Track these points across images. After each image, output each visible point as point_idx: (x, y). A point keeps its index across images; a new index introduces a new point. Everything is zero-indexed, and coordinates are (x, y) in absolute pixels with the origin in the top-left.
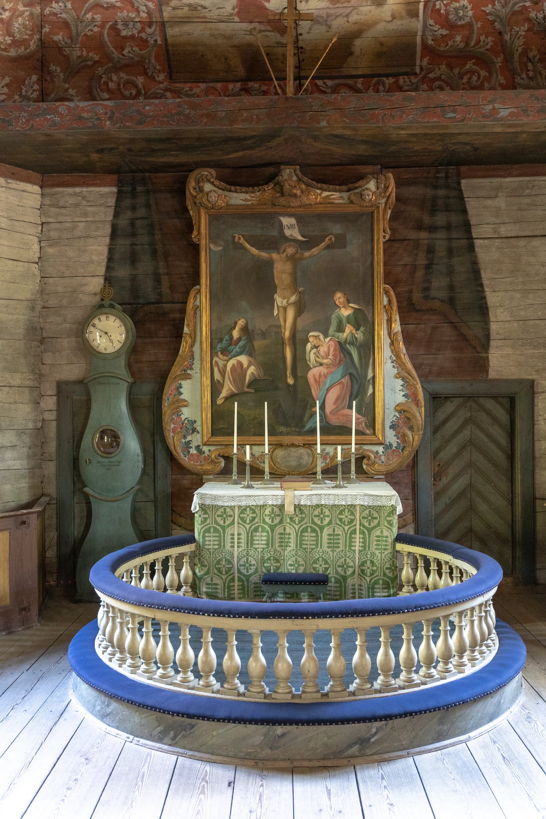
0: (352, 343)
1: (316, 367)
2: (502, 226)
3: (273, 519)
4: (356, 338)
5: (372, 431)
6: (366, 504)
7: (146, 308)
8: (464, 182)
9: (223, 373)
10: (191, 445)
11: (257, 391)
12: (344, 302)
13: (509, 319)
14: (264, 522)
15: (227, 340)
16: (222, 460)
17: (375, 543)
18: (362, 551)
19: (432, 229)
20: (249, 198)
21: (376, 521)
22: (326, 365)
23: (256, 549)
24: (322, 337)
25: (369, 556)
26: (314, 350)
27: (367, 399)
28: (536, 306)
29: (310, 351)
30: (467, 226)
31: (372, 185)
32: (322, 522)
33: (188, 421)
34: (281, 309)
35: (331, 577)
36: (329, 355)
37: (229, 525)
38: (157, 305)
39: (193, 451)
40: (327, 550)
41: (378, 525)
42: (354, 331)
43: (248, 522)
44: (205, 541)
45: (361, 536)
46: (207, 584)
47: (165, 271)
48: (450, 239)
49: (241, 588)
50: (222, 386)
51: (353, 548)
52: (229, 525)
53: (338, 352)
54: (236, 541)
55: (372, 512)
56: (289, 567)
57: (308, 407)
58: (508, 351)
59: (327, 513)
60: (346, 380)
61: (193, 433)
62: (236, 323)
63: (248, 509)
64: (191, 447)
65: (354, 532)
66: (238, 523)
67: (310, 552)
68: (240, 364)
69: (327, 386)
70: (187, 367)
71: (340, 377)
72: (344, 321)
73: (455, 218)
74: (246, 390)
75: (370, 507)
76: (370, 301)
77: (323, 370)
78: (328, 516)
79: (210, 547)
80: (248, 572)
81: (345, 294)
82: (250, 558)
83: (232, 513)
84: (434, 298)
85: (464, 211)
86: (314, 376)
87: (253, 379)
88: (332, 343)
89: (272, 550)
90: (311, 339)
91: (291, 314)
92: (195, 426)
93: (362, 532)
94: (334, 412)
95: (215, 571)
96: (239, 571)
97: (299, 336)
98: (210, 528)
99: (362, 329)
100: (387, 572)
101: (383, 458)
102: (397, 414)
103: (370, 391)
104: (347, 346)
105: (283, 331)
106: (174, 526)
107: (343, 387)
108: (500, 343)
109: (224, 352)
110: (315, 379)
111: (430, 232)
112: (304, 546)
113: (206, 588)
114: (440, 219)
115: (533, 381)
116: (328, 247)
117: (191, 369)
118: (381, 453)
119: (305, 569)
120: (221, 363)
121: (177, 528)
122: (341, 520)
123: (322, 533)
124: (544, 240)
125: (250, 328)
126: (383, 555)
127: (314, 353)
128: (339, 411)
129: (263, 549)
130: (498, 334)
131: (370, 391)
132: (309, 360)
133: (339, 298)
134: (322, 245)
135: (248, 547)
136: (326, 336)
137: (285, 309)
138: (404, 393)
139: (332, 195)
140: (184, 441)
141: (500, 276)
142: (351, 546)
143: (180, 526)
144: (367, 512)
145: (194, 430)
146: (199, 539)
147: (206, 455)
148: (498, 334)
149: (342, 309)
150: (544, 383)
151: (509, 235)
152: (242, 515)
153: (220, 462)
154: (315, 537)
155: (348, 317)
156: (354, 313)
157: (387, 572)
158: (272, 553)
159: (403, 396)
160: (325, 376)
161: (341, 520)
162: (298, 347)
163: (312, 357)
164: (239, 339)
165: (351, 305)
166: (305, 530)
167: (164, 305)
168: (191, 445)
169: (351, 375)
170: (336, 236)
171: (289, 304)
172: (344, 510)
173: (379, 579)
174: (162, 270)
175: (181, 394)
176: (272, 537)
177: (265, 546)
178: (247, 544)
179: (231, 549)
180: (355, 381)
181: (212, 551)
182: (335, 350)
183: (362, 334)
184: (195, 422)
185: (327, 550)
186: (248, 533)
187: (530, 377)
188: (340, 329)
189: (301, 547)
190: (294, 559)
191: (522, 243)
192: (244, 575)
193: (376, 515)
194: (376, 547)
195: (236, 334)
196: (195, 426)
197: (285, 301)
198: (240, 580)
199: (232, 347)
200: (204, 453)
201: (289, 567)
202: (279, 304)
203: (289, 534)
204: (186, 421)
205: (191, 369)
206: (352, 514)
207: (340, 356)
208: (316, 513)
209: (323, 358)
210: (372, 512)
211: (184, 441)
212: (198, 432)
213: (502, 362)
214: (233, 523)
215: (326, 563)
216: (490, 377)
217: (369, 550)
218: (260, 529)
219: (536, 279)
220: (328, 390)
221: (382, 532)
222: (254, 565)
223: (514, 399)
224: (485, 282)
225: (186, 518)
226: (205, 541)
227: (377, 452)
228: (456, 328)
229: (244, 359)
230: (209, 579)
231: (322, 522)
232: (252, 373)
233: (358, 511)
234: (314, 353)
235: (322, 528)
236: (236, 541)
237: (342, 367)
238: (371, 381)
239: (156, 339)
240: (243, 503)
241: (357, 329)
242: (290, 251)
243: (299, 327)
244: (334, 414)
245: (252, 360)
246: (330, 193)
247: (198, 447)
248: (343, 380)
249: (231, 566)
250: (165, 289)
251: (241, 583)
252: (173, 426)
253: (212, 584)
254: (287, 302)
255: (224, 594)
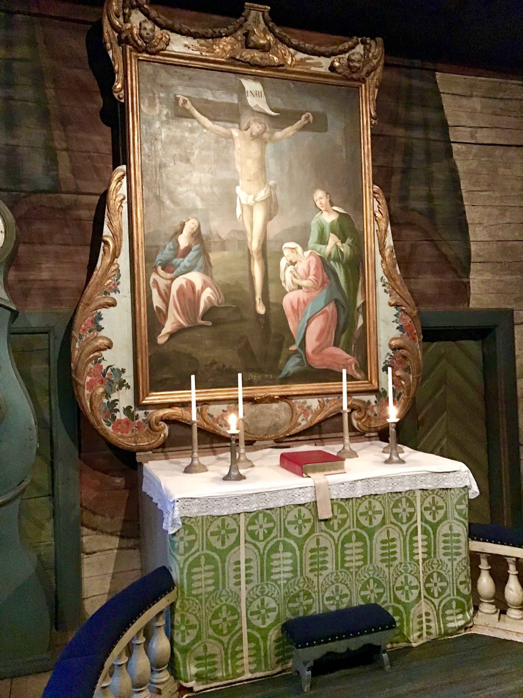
0: (337, 260)
1: (293, 290)
2: (479, 130)
3: (300, 528)
4: (342, 253)
5: (363, 374)
6: (429, 487)
7: (33, 198)
8: (438, 75)
9: (165, 298)
10: (117, 407)
11: (216, 323)
12: (326, 203)
13: (488, 239)
14: (287, 534)
15: (170, 249)
16: (163, 424)
17: (443, 545)
18: (427, 559)
19: (409, 125)
20: (198, 45)
21: (441, 512)
22: (307, 288)
23: (276, 581)
24: (299, 249)
25: (435, 566)
26: (291, 268)
27: (357, 334)
28: (513, 226)
29: (285, 269)
30: (444, 126)
31: (360, 49)
32: (371, 523)
33: (113, 370)
34: (245, 208)
35: (388, 607)
36: (309, 275)
37: (231, 547)
38: (52, 195)
39: (121, 416)
40: (380, 565)
41: (445, 517)
42: (339, 244)
43: (261, 537)
44: (193, 581)
45: (425, 537)
46: (198, 659)
47: (64, 145)
48: (428, 140)
49: (253, 652)
50: (165, 317)
51: (416, 558)
52: (231, 547)
53: (320, 271)
54: (243, 573)
55: (437, 498)
56: (326, 603)
57: (285, 345)
58: (488, 276)
59: (378, 507)
60: (331, 308)
61: (120, 388)
62: (183, 225)
63: (261, 516)
64: (118, 410)
65: (415, 532)
66: (246, 542)
67: (356, 573)
68: (192, 285)
69: (307, 317)
70: (110, 288)
71: (323, 304)
72: (327, 230)
73: (433, 116)
74: (200, 322)
75: (433, 490)
76: (358, 205)
77: (301, 295)
78: (380, 512)
79: (200, 591)
80: (264, 623)
81: (327, 194)
82: (266, 599)
83: (235, 526)
84: (413, 210)
85: (441, 108)
86: (291, 303)
87: (209, 306)
88: (312, 258)
89: (302, 580)
90: (286, 252)
91: (259, 215)
92: (123, 377)
93: (425, 532)
94: (318, 351)
95: (211, 631)
96: (250, 624)
97: (270, 247)
98: (199, 558)
99: (349, 241)
100: (461, 587)
101: (375, 409)
102: (391, 352)
103: (360, 322)
104: (332, 263)
105: (249, 239)
106: (85, 530)
107: (327, 318)
108: (478, 266)
109: (167, 266)
110: (293, 307)
111: (406, 129)
112: (347, 565)
113: (197, 666)
114: (417, 114)
115: (512, 311)
116: (304, 128)
117: (116, 291)
118: (373, 403)
119: (350, 600)
120: (162, 283)
121: (90, 531)
122: (396, 515)
123: (371, 539)
124: (520, 150)
125: (203, 231)
126: (455, 563)
127: (291, 272)
128: (323, 349)
129: (288, 580)
130: (479, 256)
131: (360, 322)
132: (285, 281)
133: (321, 198)
134: (298, 124)
135: (262, 581)
136: (305, 248)
137: (251, 208)
138: (398, 325)
139: (309, 59)
140: (105, 401)
141: (478, 189)
142: (412, 555)
143: (94, 529)
144: (430, 499)
145: (122, 384)
146: (182, 580)
147: (140, 420)
148: (479, 256)
149: (324, 213)
150: (520, 315)
151: (485, 142)
152: (251, 528)
153: (164, 428)
154: (362, 547)
155: (332, 224)
156: (338, 219)
157: (461, 587)
158: (301, 585)
159: (398, 328)
160: (305, 303)
161: (396, 515)
162: (270, 262)
163: (287, 276)
164: (188, 250)
165: (335, 208)
166: (347, 539)
167: (63, 196)
168: (117, 407)
169: (336, 301)
170: (314, 114)
171: (256, 202)
172: (400, 500)
173: (452, 600)
174: (59, 144)
175: (100, 329)
176: (301, 557)
177: (290, 575)
178: (262, 575)
179: (235, 589)
180: (341, 310)
181: (203, 597)
182: (316, 268)
183: (348, 247)
184: (123, 371)
185: (380, 565)
186: (262, 556)
187: (509, 307)
188: (322, 240)
189: (342, 566)
190: (333, 588)
191: (498, 152)
192: (259, 630)
193: (441, 503)
194: (444, 551)
195: (183, 241)
196: (123, 377)
197: (252, 197)
198: (251, 638)
199: (177, 261)
200: (137, 417)
201: (326, 603)
202: (244, 202)
203: (326, 548)
204: (109, 371)
205: (116, 291)
206: (412, 505)
207: (323, 276)
208: (362, 509)
209: (302, 279)
210: (437, 498)
211: (105, 401)
212: (128, 387)
213: (483, 290)
214: (237, 542)
215: (379, 585)
216: (471, 306)
217: (435, 557)
218: (281, 548)
219: (513, 194)
220: (309, 322)
221: (451, 528)
222: (274, 610)
223: (487, 331)
224: (464, 195)
225: (103, 516)
226: (193, 581)
227: (369, 403)
228: (436, 247)
229: (196, 277)
230: (201, 648)
231: (371, 523)
232: (209, 298)
233: (418, 499)
234: (291, 272)
235: (371, 533)
236: (243, 573)
237: (325, 291)
238: (361, 310)
239: (50, 248)
240: (254, 507)
241: (343, 242)
242: (256, 128)
243: (271, 236)
244: (317, 354)
245: (208, 279)
246: (306, 56)
247: (127, 410)
248: (327, 308)
249: (236, 617)
250: (64, 171)
251: (253, 645)
252: (88, 379)
253: (206, 657)
254: (254, 199)
255: (227, 670)
